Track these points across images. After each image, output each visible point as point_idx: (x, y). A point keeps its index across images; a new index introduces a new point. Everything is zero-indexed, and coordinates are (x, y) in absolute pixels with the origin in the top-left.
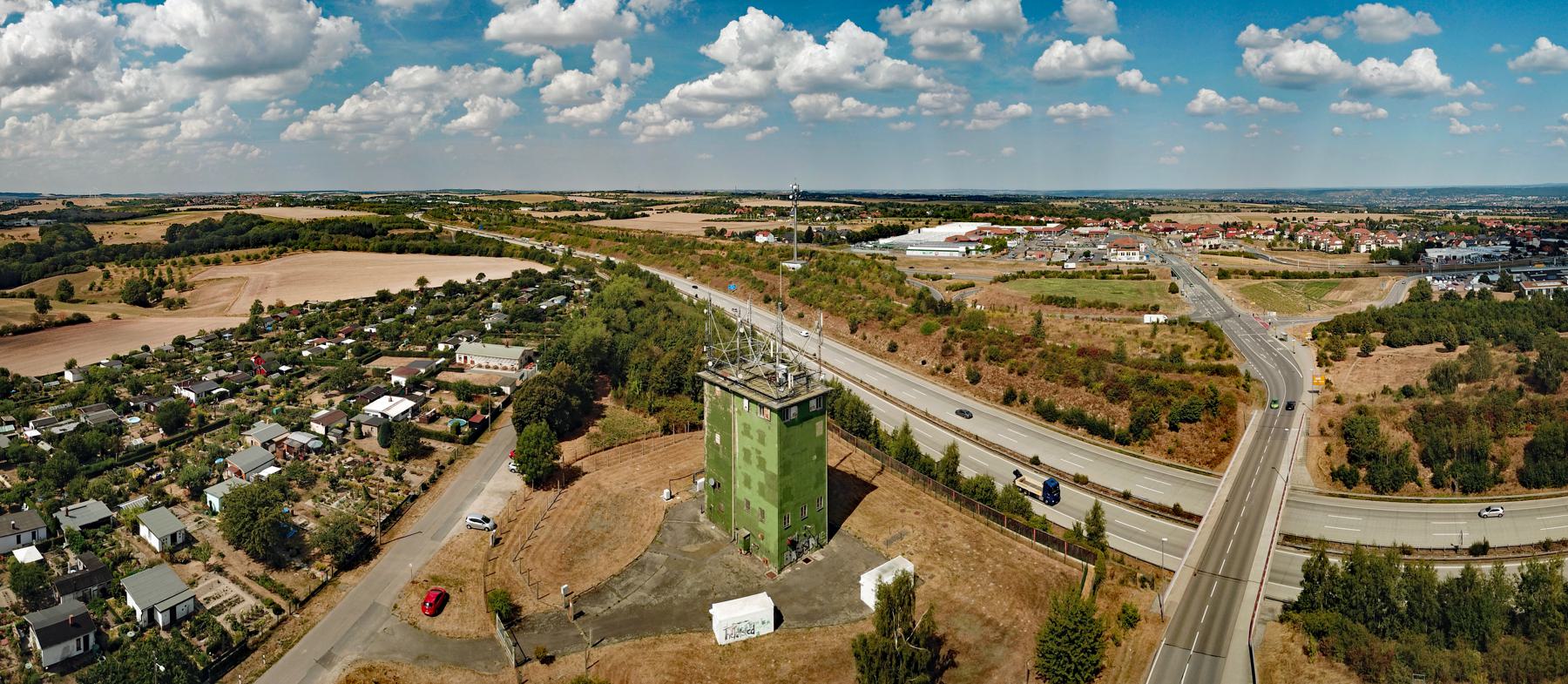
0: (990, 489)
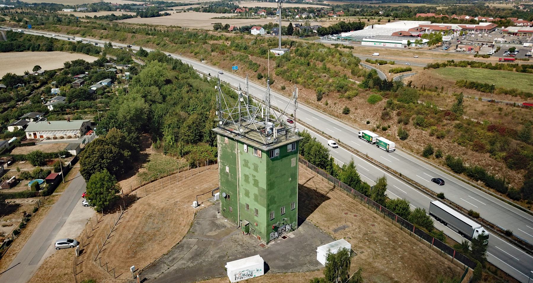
0: (406, 208)
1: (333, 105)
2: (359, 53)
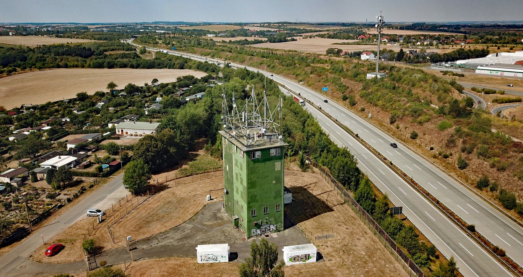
1: (403, 129)
2: (469, 81)
